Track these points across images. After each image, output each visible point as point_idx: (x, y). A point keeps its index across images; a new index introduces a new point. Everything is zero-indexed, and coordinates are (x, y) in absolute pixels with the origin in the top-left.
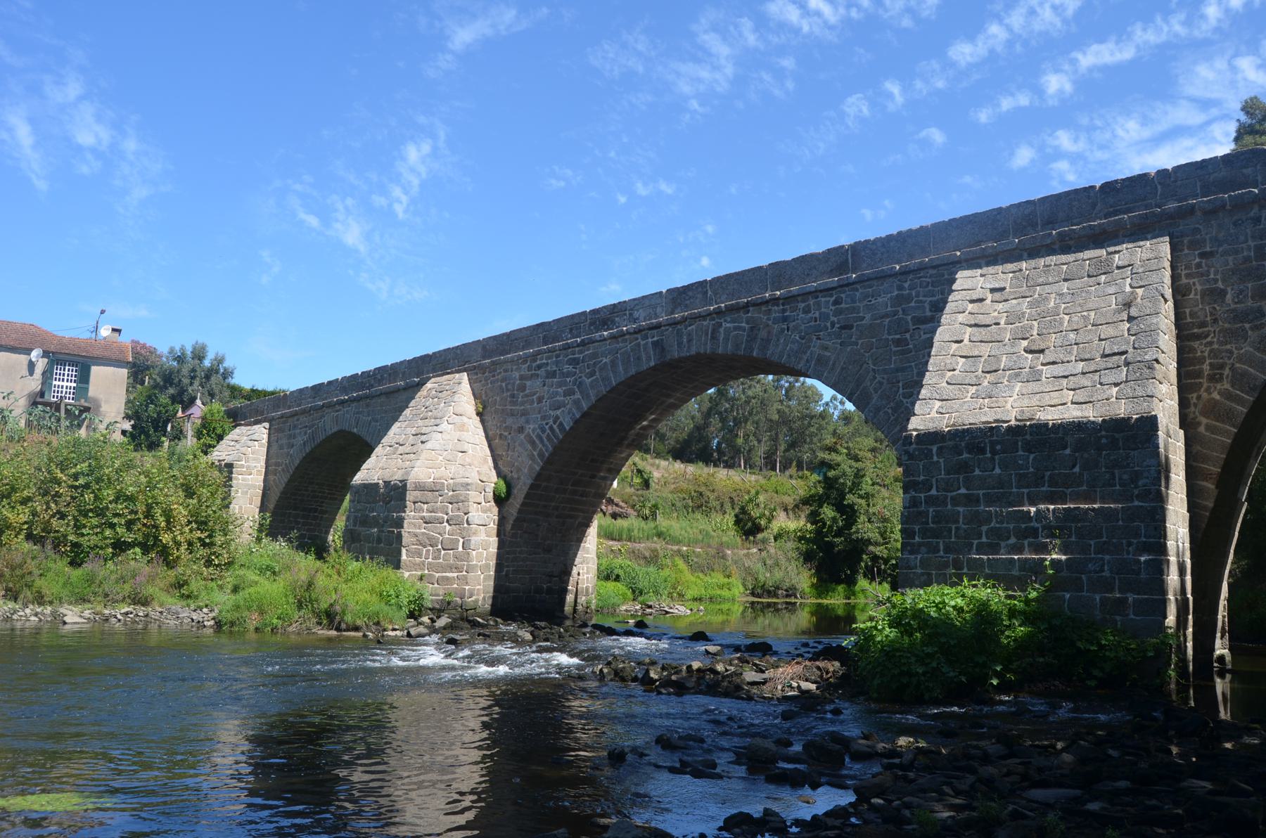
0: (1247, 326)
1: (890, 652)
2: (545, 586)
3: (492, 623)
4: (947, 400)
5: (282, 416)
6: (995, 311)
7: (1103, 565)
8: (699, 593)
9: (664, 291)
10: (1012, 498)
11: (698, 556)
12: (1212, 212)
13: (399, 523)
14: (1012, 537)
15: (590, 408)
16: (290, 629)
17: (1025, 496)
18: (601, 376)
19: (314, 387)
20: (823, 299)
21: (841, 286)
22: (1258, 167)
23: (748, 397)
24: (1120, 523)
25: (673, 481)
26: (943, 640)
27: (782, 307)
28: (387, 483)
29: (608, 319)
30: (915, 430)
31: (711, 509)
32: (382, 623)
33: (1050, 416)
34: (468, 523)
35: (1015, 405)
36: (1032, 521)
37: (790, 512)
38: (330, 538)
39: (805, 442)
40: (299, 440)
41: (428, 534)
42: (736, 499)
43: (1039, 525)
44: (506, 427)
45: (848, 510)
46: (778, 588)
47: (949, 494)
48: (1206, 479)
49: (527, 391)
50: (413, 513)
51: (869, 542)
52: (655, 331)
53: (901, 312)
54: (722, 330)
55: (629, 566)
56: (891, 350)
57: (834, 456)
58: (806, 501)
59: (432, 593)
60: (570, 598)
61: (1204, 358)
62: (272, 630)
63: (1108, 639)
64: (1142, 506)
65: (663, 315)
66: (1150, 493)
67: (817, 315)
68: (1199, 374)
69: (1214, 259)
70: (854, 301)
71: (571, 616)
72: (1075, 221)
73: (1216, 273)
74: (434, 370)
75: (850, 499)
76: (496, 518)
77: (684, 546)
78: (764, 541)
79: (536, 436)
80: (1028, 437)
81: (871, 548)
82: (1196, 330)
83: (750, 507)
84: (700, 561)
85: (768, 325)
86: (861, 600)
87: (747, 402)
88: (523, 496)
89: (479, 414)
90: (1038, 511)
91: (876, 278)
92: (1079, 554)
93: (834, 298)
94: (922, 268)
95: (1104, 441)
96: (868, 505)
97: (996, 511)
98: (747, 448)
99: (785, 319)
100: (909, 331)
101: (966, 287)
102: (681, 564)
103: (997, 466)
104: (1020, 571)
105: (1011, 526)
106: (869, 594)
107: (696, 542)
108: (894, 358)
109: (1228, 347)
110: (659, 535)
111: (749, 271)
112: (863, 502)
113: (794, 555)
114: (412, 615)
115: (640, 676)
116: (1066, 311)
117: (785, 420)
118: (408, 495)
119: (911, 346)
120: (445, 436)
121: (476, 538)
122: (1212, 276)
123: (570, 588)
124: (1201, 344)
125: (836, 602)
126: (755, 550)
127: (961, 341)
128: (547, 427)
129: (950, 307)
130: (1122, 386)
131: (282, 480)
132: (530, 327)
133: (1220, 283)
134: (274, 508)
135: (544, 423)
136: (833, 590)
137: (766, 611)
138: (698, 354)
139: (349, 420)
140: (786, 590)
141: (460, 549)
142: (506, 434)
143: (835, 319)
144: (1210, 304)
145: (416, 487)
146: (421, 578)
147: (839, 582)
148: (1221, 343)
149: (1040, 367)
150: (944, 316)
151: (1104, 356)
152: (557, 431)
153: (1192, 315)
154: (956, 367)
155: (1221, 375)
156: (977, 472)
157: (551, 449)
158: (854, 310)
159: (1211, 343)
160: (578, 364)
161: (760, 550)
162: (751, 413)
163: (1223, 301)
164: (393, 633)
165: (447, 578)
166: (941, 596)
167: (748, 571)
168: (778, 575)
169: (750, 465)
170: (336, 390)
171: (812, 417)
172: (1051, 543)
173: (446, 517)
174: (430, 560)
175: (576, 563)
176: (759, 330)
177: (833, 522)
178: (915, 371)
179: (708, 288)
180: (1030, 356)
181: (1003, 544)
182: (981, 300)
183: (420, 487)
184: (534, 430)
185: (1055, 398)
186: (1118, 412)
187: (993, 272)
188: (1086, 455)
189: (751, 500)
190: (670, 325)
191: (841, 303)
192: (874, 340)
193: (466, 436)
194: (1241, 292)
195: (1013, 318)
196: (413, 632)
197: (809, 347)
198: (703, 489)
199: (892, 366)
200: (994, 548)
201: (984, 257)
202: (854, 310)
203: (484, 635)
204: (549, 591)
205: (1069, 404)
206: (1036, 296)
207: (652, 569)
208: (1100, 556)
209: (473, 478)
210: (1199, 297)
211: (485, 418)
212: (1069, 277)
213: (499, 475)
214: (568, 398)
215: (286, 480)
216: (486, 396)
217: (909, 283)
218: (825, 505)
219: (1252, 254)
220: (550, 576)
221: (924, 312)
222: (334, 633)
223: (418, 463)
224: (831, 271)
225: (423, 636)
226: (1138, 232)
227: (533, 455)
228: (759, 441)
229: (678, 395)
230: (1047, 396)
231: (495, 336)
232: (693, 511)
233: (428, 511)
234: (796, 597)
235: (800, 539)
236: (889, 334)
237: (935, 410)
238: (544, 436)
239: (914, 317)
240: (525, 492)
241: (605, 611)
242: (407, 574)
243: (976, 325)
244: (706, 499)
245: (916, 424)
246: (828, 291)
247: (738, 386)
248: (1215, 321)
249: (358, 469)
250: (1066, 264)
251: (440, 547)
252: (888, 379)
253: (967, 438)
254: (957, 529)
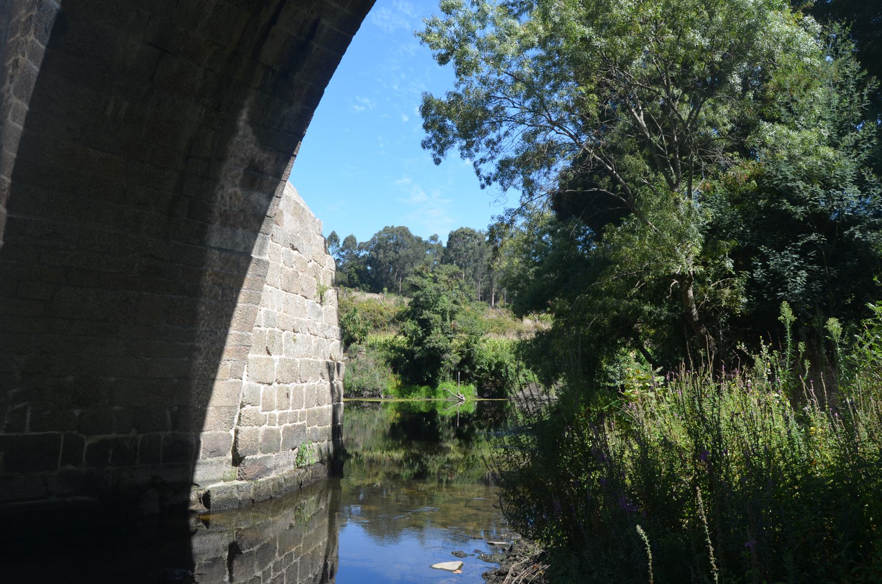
147: (422, 384)
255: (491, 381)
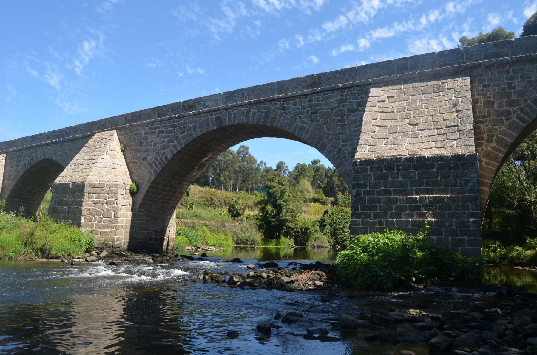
0: (504, 118)
1: (366, 266)
3: (129, 255)
5: (13, 151)
6: (390, 106)
7: (452, 223)
9: (222, 93)
10: (407, 191)
11: (213, 226)
12: (488, 67)
13: (80, 204)
14: (408, 210)
15: (182, 149)
16: (20, 258)
17: (414, 191)
19: (32, 137)
20: (303, 99)
21: (312, 93)
22: (509, 48)
23: (226, 160)
24: (460, 203)
26: (390, 259)
27: (282, 102)
28: (74, 183)
29: (192, 106)
32: (72, 255)
33: (426, 153)
34: (117, 204)
35: (407, 148)
36: (418, 203)
37: (250, 208)
38: (37, 213)
39: (249, 180)
40: (23, 163)
41: (96, 210)
42: (227, 202)
43: (421, 204)
44: (136, 158)
46: (247, 240)
48: (485, 186)
49: (148, 140)
50: (88, 199)
51: (287, 221)
52: (217, 112)
53: (342, 106)
54: (251, 112)
58: (259, 203)
59: (98, 240)
60: (165, 243)
61: (485, 132)
62: (9, 258)
63: (460, 257)
64: (470, 196)
65: (221, 104)
66: (474, 190)
67: (300, 106)
68: (482, 139)
69: (489, 88)
70: (318, 101)
72: (426, 68)
73: (490, 94)
74: (98, 129)
75: (279, 202)
76: (131, 202)
78: (241, 220)
79: (153, 162)
80: (415, 163)
81: (288, 223)
82: (481, 119)
83: (236, 204)
85: (275, 111)
86: (282, 246)
87: (226, 162)
88: (145, 192)
89: (122, 151)
90: (421, 198)
91: (330, 90)
92: (440, 218)
93: (308, 99)
94: (353, 86)
95: (452, 165)
96: (287, 205)
97: (400, 198)
99: (284, 108)
100: (345, 116)
101: (376, 95)
102: (206, 229)
103: (400, 177)
104: (412, 226)
105: (407, 205)
106: (286, 243)
107: (212, 219)
109: (495, 127)
110: (196, 216)
111: (266, 85)
112: (285, 203)
114: (87, 251)
115: (227, 280)
116: (426, 107)
117: (241, 170)
118: (85, 189)
120: (105, 160)
121: (121, 212)
122: (488, 95)
123: (165, 238)
124: (483, 125)
126: (238, 224)
127: (376, 119)
129: (368, 104)
130: (458, 140)
131: (12, 183)
132: (151, 109)
133: (492, 98)
134: (8, 198)
136: (271, 242)
138: (239, 124)
139: (51, 153)
140: (251, 242)
141: (113, 217)
142: (137, 161)
143: (309, 109)
144: (487, 108)
145: (90, 185)
146: (92, 232)
147: (273, 238)
148: (492, 125)
149: (417, 132)
150: (366, 108)
151: (447, 127)
152: (164, 160)
153: (479, 112)
155: (492, 139)
156: (390, 179)
158: (318, 105)
159: (488, 125)
160: (176, 127)
162: (227, 167)
163: (493, 107)
164: (78, 260)
165: (106, 232)
166: (377, 239)
167: (235, 233)
168: (247, 235)
170: (44, 138)
171: (253, 170)
172: (427, 213)
173: (105, 201)
174: (96, 223)
176: (270, 113)
178: (348, 134)
179: (245, 92)
180: (411, 127)
181: (403, 213)
182: (384, 101)
183: (92, 186)
184: (151, 159)
185: (427, 145)
186: (458, 152)
187: (388, 89)
188: (443, 172)
189: (236, 202)
190: (225, 109)
191: (312, 101)
193: (116, 161)
194: (501, 103)
195: (400, 110)
196: (89, 259)
197: (296, 122)
198: (213, 197)
199: (337, 132)
200: (399, 215)
201: (383, 82)
202: (318, 105)
203: (128, 260)
204: (156, 239)
205: (434, 148)
206: (410, 100)
207: (194, 231)
208: (451, 219)
209: (120, 182)
210: (482, 104)
211: (126, 153)
212: (424, 92)
213: (133, 181)
215: (15, 183)
216: (126, 142)
217: (346, 93)
219: (506, 86)
221: (353, 107)
222: (45, 260)
223: (91, 173)
224: (308, 86)
225: (95, 261)
226: (457, 74)
227: (151, 171)
228: (230, 179)
229: (224, 145)
230: (422, 145)
231: (132, 113)
233: (96, 198)
235: (257, 219)
236: (336, 116)
238: (157, 162)
239: (348, 109)
240: (146, 190)
241: (179, 249)
242: (84, 230)
243: (383, 112)
245: (358, 156)
246: (306, 95)
248: (490, 115)
249: (57, 176)
250: (422, 87)
251: (102, 216)
252: (335, 138)
254: (380, 206)
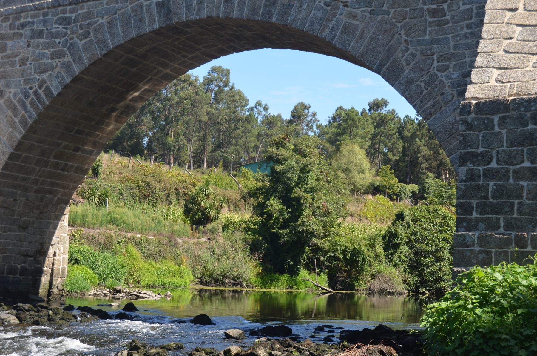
2: (19, 266)
4: (507, 68)
8: (152, 280)
11: (151, 243)
15: (82, 73)
18: (95, 38)
25: (118, 171)
30: (474, 98)
31: (157, 199)
42: (181, 191)
45: (294, 203)
46: (225, 277)
47: (511, 167)
51: (312, 234)
55: (88, 250)
56: (426, 20)
57: (282, 151)
58: (253, 194)
60: (45, 280)
71: (46, 299)
75: (297, 192)
77: (138, 233)
78: (212, 231)
81: (314, 240)
84: (153, 249)
96: (313, 199)
98: (177, 147)
107: (149, 229)
108: (428, 29)
112: (309, 196)
113: (241, 245)
117: (214, 122)
119: (448, 17)
123: (45, 269)
125: (279, 291)
126: (204, 240)
127: (515, 10)
128: (31, 92)
135: (28, 87)
136: (277, 280)
137: (213, 299)
138: (210, 18)
140: (233, 279)
147: (282, 272)
152: (43, 96)
154: (512, 36)
157: (35, 115)
160: (69, 24)
161: (209, 239)
162: (182, 114)
166: (513, 276)
167: (198, 260)
168: (226, 264)
169: (180, 164)
171: (238, 121)
175: (52, 243)
177: (280, 214)
184: (15, 95)
189: (201, 191)
192: (408, 9)
197: (335, 15)
198: (150, 179)
204: (24, 272)
214: (57, 60)
218: (272, 198)
220: (25, 256)
227: (14, 122)
228: (189, 141)
232: (140, 201)
234: (242, 286)
237: (494, 78)
238: (27, 102)
241: (74, 294)
244: (153, 189)
247: (171, 87)
252: (421, 51)
253: (533, 108)
254: (520, 204)
255: (345, 271)
